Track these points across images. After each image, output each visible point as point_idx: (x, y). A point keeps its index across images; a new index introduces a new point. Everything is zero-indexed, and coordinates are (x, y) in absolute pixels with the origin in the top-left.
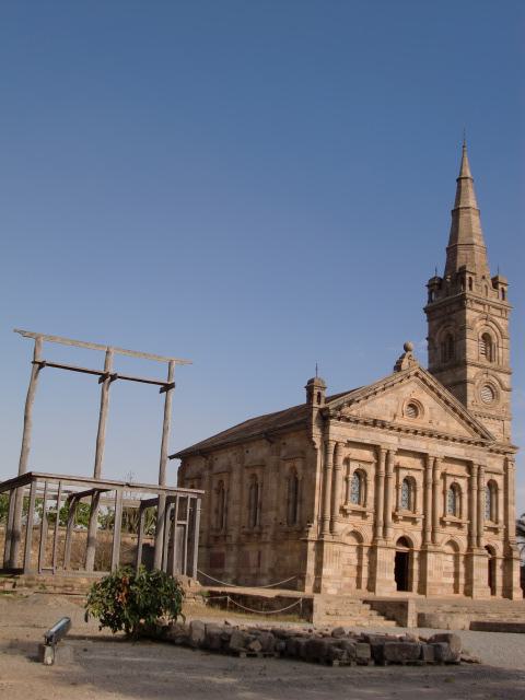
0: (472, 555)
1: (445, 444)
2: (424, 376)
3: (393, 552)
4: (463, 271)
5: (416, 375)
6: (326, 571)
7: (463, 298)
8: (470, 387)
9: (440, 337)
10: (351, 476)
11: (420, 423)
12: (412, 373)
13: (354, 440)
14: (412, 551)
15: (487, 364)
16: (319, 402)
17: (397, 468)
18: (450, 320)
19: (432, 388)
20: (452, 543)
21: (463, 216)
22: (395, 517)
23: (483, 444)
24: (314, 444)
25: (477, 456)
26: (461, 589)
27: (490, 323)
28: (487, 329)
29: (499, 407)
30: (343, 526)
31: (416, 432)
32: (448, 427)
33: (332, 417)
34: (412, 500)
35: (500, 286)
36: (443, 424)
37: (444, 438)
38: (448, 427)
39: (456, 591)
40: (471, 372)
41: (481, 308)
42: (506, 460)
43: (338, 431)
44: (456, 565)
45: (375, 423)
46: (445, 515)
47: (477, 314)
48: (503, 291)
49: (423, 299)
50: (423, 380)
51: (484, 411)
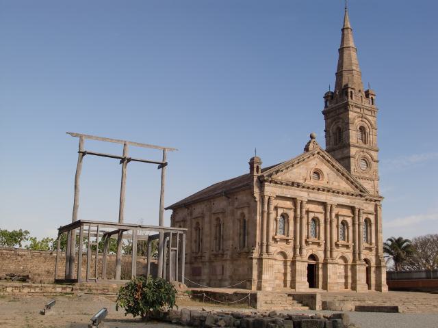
5: (318, 153)
9: (333, 128)
11: (322, 183)
15: (363, 145)
18: (339, 118)
23: (361, 196)
31: (319, 189)
41: (358, 110)
51: (362, 175)
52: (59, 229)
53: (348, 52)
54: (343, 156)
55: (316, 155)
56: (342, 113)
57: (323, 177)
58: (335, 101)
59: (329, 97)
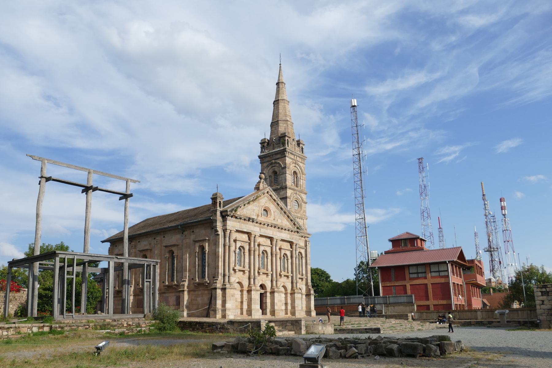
0: (251, 290)
1: (281, 232)
2: (272, 194)
3: (259, 293)
4: (283, 136)
5: (268, 192)
6: (228, 305)
7: (285, 150)
8: (288, 200)
10: (238, 250)
11: (270, 220)
12: (266, 192)
13: (239, 229)
14: (266, 292)
15: (296, 188)
16: (220, 206)
17: (259, 245)
19: (275, 200)
20: (284, 287)
21: (281, 105)
22: (280, 275)
23: (298, 232)
24: (217, 231)
25: (295, 238)
26: (245, 312)
27: (297, 166)
28: (295, 169)
29: (302, 212)
30: (234, 279)
32: (282, 222)
33: (228, 216)
34: (266, 263)
35: (301, 146)
36: (280, 221)
37: (281, 228)
38: (282, 222)
39: (286, 314)
40: (289, 192)
42: (306, 241)
43: (231, 224)
44: (286, 298)
45: (249, 219)
46: (235, 266)
48: (302, 148)
50: (271, 196)
55: (266, 194)
59: (264, 144)
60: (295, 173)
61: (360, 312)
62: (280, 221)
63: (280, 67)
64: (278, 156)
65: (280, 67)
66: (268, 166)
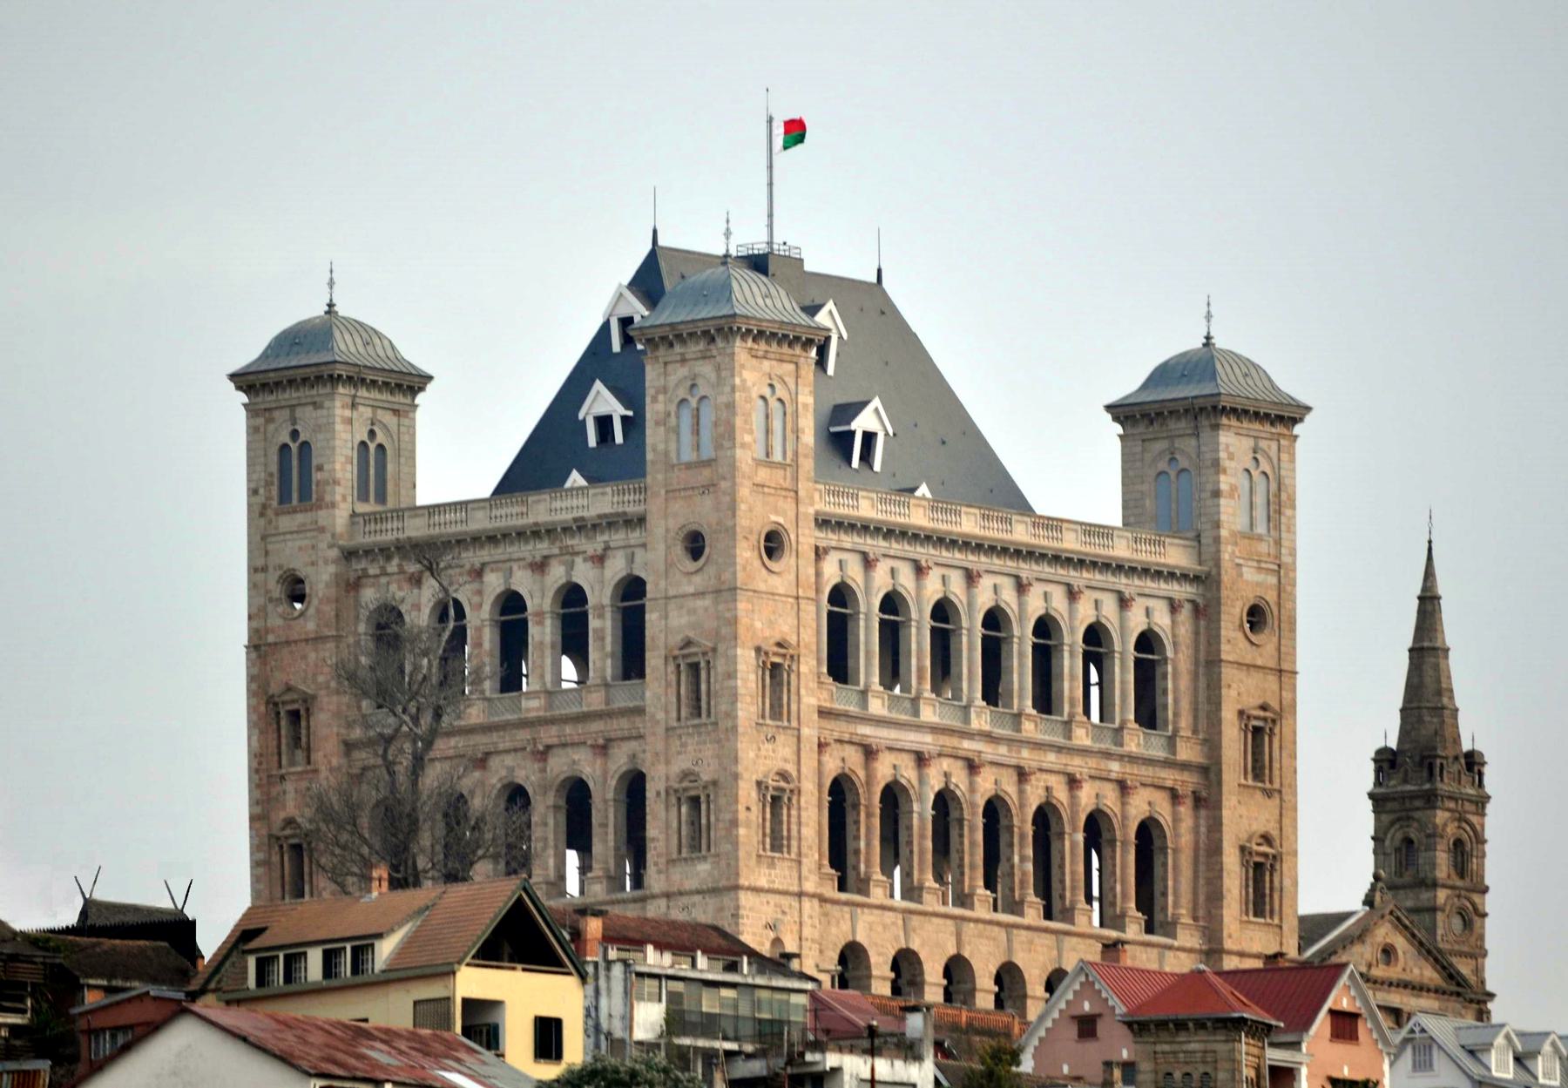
1: (1419, 996)
5: (1391, 913)
9: (1394, 838)
11: (1394, 973)
15: (1459, 883)
18: (1409, 818)
23: (1458, 994)
29: (1473, 940)
31: (1391, 984)
41: (1452, 805)
47: (1447, 814)
49: (1366, 777)
50: (1398, 919)
51: (1456, 947)
52: (194, 922)
53: (1433, 660)
54: (1419, 904)
55: (1388, 917)
56: (1418, 809)
57: (1397, 959)
58: (1401, 775)
59: (1385, 761)
60: (1458, 843)
61: (802, 1055)
62: (1416, 971)
63: (1430, 549)
64: (1418, 803)
65: (1430, 549)
66: (1392, 823)
